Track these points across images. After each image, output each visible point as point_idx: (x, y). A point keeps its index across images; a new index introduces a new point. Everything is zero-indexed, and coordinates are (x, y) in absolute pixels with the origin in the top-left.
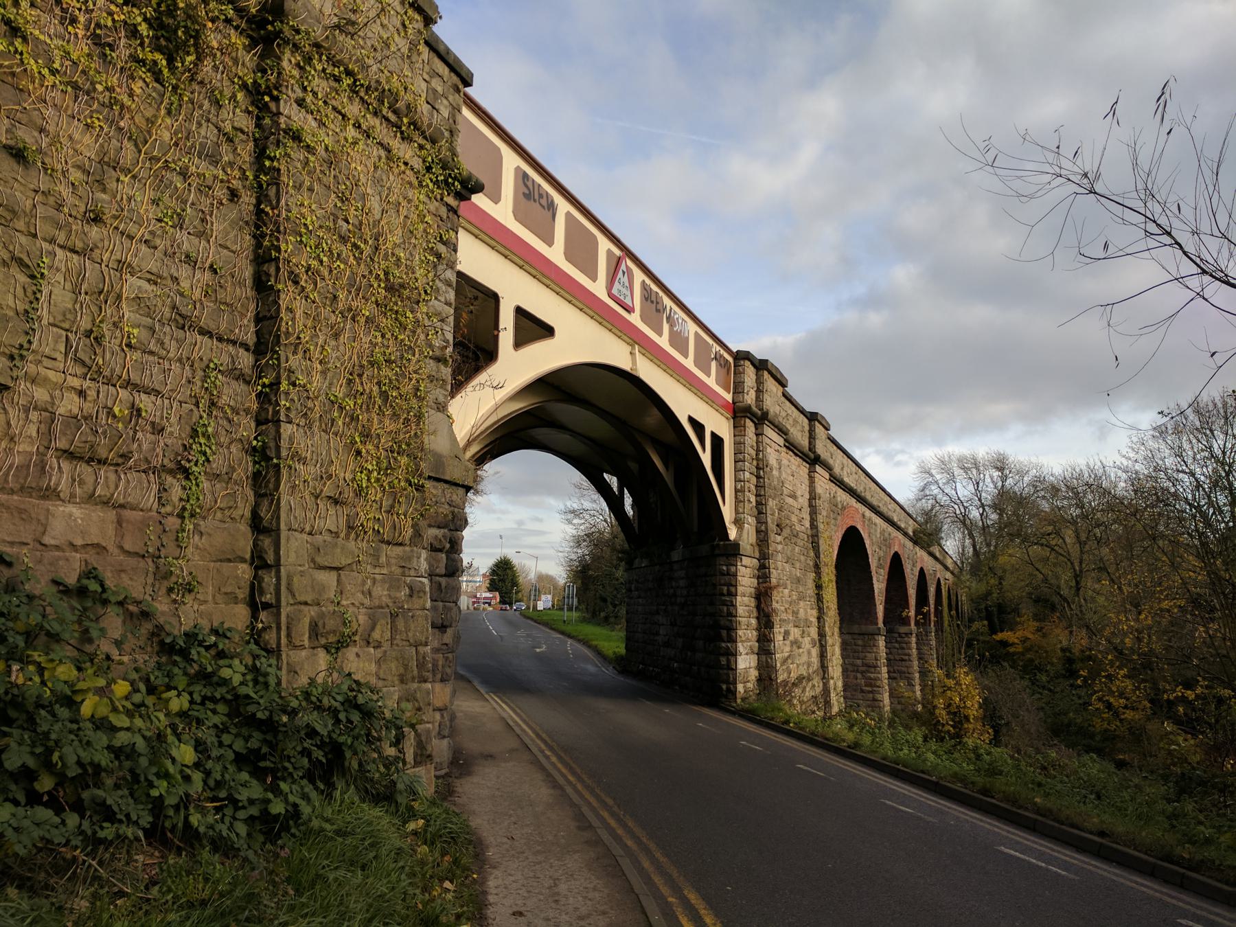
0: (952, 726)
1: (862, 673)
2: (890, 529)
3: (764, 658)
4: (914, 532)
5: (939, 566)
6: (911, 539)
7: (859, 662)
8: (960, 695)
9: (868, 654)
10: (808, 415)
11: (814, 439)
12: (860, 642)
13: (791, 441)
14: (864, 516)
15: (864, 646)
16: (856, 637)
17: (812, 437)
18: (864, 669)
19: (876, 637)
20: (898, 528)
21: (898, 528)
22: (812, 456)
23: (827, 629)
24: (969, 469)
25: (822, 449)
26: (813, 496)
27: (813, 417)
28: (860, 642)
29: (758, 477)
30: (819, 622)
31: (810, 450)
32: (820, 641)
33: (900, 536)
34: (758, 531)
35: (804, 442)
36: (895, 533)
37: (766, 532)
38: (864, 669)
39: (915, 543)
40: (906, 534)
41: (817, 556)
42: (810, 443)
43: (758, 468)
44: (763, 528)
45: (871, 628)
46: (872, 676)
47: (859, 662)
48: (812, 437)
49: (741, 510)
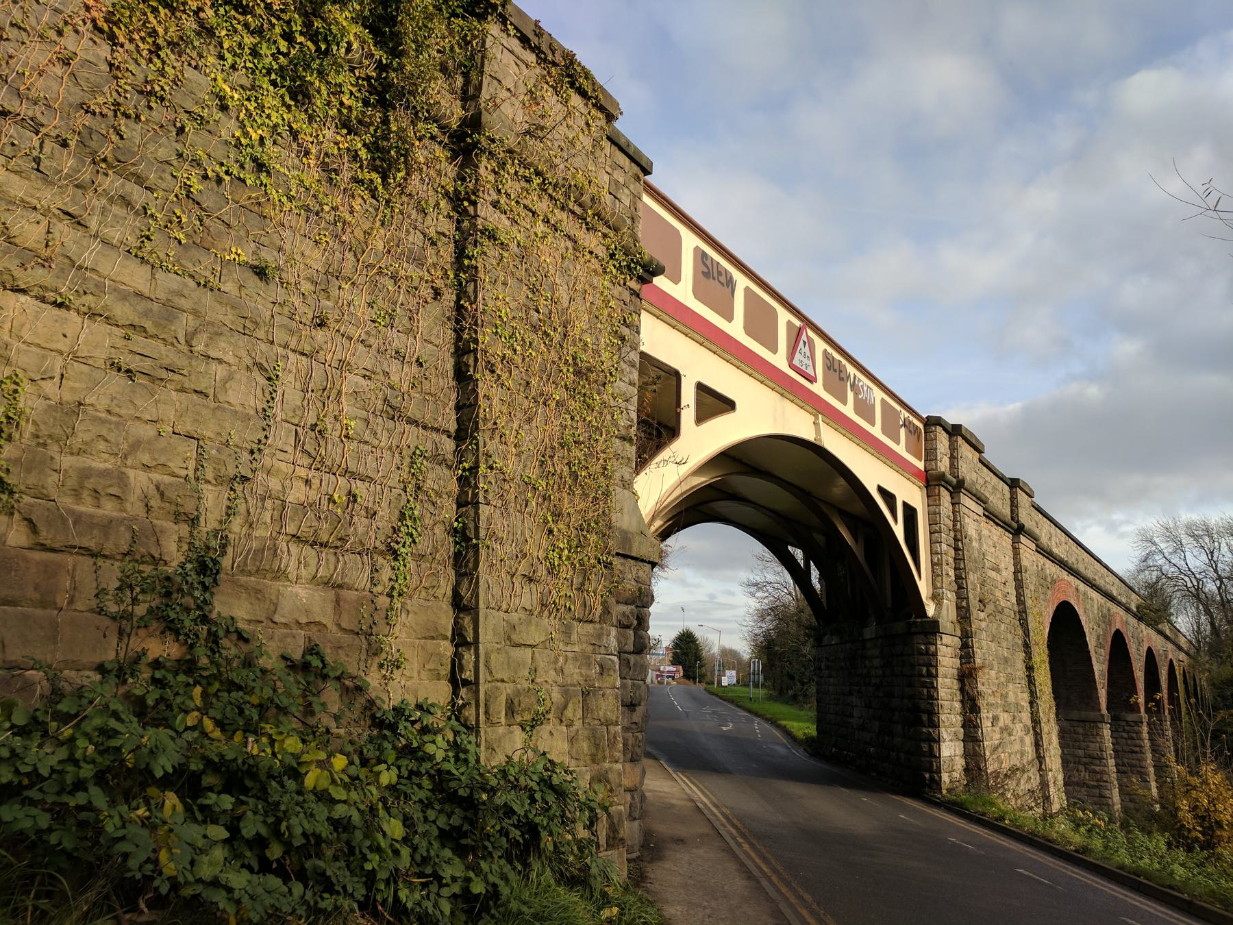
0: (1200, 832)
1: (1085, 764)
2: (1110, 604)
3: (970, 745)
4: (1138, 608)
5: (1170, 646)
6: (1135, 616)
7: (1081, 752)
8: (1209, 796)
9: (1091, 744)
10: (1009, 482)
11: (1017, 507)
12: (1080, 730)
13: (991, 510)
14: (1077, 590)
15: (1086, 735)
16: (1075, 724)
17: (1014, 505)
18: (1087, 760)
19: (1100, 725)
20: (1119, 603)
21: (1119, 603)
22: (1015, 525)
23: (1041, 714)
24: (1200, 536)
25: (1027, 517)
26: (1018, 570)
27: (1014, 484)
28: (1080, 730)
29: (956, 549)
30: (1031, 707)
31: (1012, 519)
32: (1034, 728)
33: (1121, 612)
34: (959, 608)
35: (1006, 511)
36: (1115, 609)
37: (968, 609)
38: (1087, 760)
39: (1140, 619)
40: (1128, 610)
41: (1026, 633)
42: (1012, 511)
43: (956, 539)
44: (964, 604)
45: (1093, 715)
46: (1097, 768)
47: (1081, 752)
48: (1014, 505)
49: (939, 585)
